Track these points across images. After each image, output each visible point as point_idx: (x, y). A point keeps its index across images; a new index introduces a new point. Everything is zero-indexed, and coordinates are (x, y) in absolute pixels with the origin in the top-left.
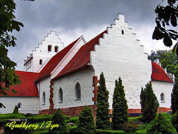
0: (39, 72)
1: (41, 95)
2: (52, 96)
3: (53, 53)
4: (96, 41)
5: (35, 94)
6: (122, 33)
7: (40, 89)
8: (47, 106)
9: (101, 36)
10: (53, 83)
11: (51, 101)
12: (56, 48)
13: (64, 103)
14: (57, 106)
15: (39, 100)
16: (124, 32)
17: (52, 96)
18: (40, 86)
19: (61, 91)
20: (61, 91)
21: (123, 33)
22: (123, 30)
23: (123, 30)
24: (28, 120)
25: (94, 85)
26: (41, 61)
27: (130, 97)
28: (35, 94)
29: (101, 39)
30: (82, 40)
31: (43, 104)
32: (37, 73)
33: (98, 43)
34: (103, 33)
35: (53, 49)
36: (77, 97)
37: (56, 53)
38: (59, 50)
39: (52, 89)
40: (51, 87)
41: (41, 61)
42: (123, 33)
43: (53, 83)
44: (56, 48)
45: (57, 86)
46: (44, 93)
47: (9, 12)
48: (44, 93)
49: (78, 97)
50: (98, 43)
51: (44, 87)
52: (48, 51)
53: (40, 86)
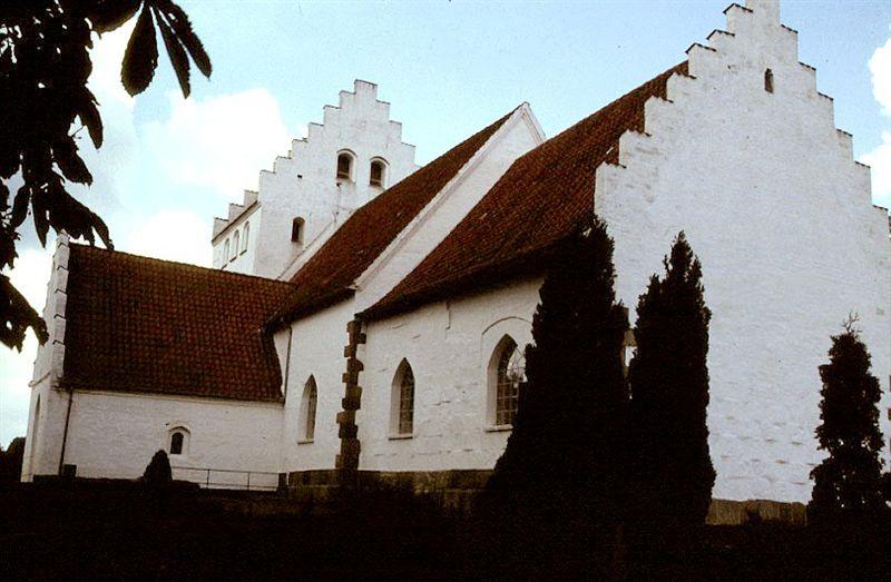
0: (287, 278)
1: (294, 392)
2: (352, 402)
3: (362, 193)
4: (626, 114)
5: (264, 385)
6: (764, 87)
7: (290, 371)
8: (324, 454)
9: (657, 87)
10: (364, 336)
11: (348, 430)
12: (377, 169)
13: (416, 445)
14: (381, 455)
15: (283, 414)
16: (777, 80)
17: (352, 402)
18: (289, 348)
19: (405, 375)
20: (405, 375)
21: (769, 87)
22: (768, 70)
23: (768, 70)
24: (637, 130)
25: (667, 268)
26: (298, 225)
27: (795, 439)
28: (264, 385)
29: (652, 105)
30: (522, 124)
31: (303, 439)
32: (276, 281)
33: (638, 126)
34: (668, 74)
35: (360, 170)
36: (498, 415)
37: (375, 193)
38: (391, 178)
39: (355, 367)
40: (351, 352)
41: (298, 225)
42: (769, 87)
43: (362, 332)
44: (377, 169)
45: (387, 347)
46: (311, 385)
47: (17, 28)
48: (311, 385)
49: (503, 418)
50: (638, 126)
51: (313, 349)
52: (339, 176)
53: (289, 348)
